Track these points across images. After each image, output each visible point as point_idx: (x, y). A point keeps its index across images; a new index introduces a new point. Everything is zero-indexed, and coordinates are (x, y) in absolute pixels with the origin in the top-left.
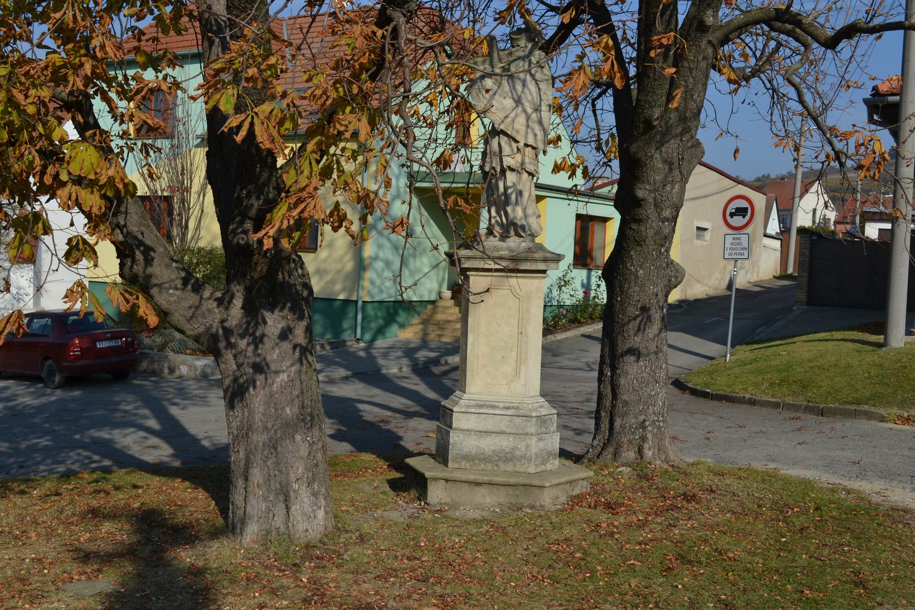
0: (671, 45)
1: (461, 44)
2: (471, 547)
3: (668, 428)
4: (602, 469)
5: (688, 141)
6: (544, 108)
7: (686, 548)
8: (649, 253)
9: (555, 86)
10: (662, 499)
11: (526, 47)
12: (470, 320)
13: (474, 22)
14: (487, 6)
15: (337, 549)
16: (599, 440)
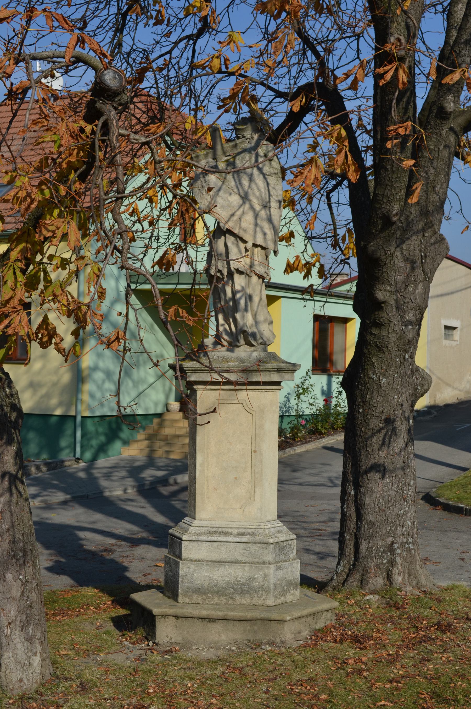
0: (409, 136)
1: (182, 135)
2: (205, 692)
3: (418, 550)
4: (348, 598)
5: (431, 237)
6: (274, 204)
7: (441, 685)
8: (392, 359)
9: (286, 178)
10: (414, 630)
11: (252, 138)
12: (199, 439)
13: (196, 110)
14: (210, 93)
15: (56, 699)
16: (344, 566)
